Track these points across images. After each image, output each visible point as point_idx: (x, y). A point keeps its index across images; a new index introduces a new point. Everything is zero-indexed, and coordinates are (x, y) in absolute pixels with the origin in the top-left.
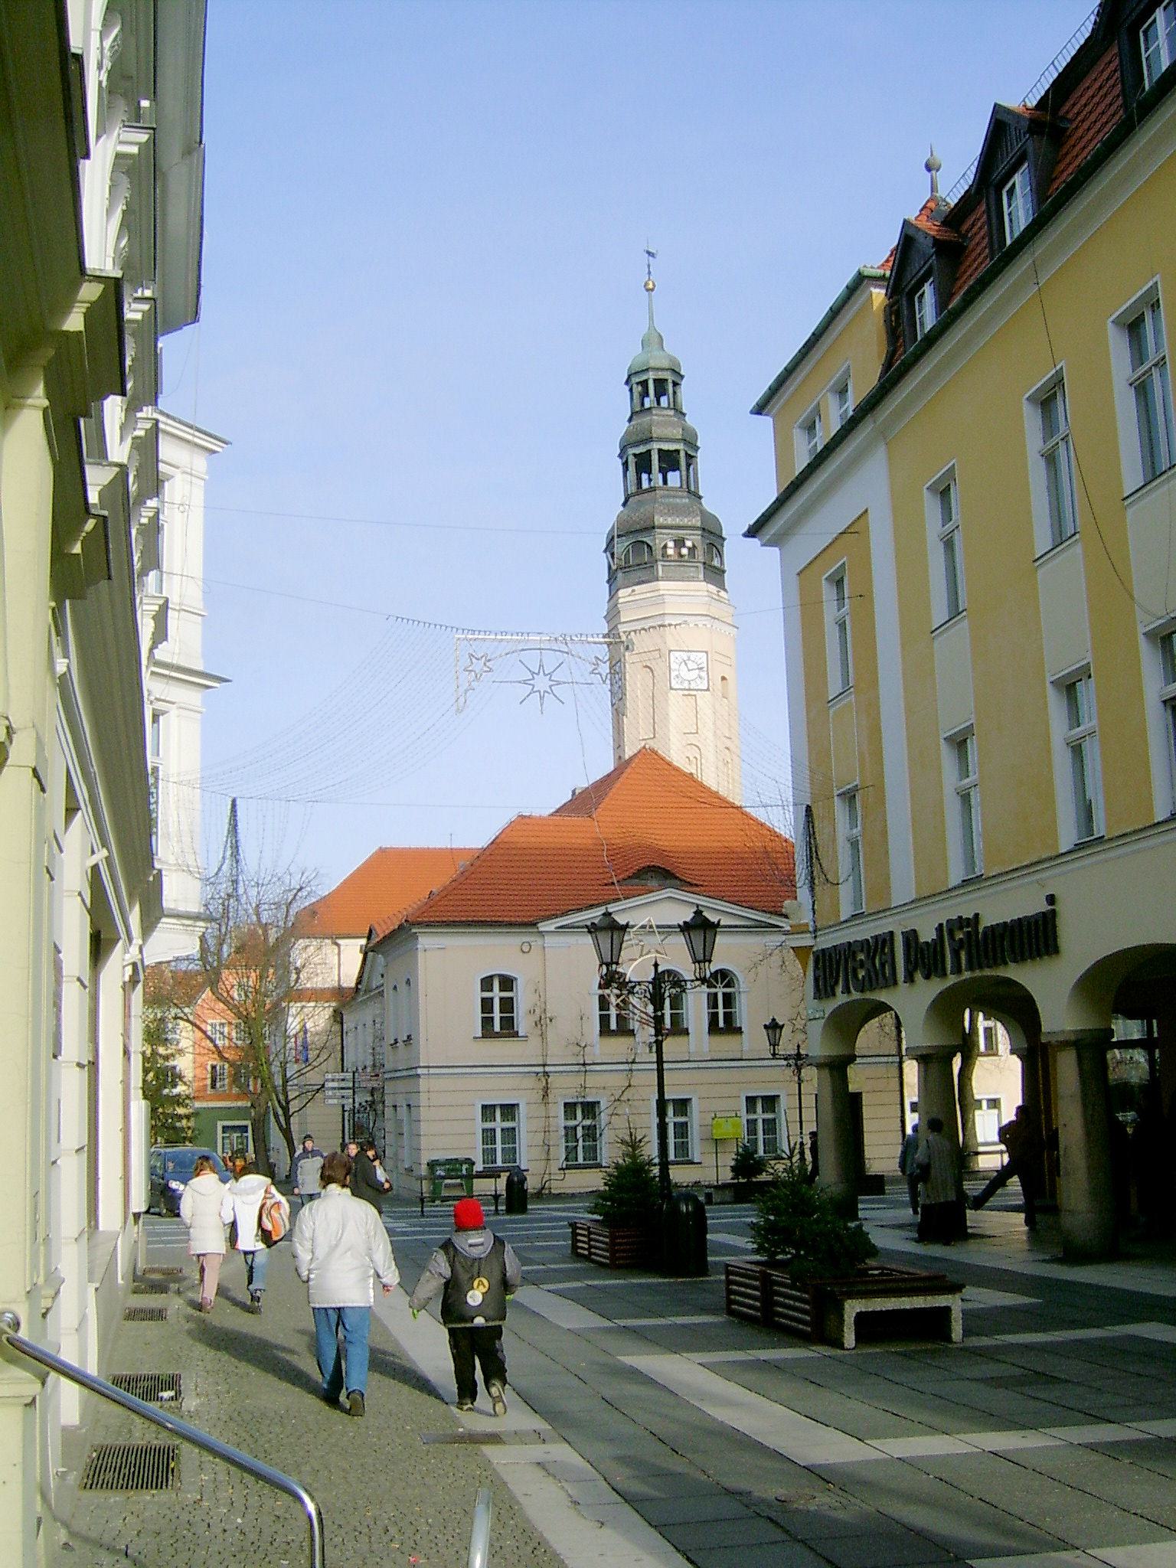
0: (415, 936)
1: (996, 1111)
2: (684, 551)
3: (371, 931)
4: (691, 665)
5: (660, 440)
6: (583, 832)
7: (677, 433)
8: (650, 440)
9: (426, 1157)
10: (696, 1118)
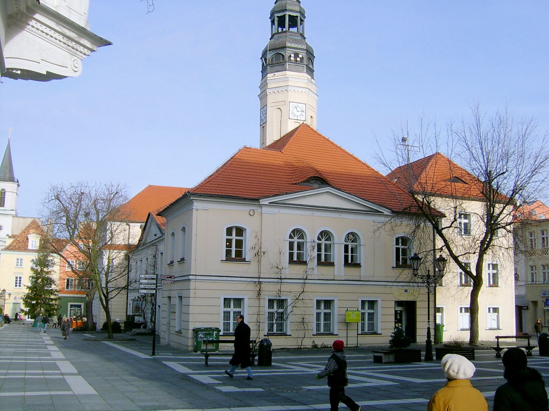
0: (191, 202)
1: (496, 314)
2: (298, 59)
3: (149, 215)
4: (299, 109)
5: (290, 11)
6: (277, 159)
7: (298, 9)
8: (286, 10)
9: (192, 326)
10: (337, 310)
